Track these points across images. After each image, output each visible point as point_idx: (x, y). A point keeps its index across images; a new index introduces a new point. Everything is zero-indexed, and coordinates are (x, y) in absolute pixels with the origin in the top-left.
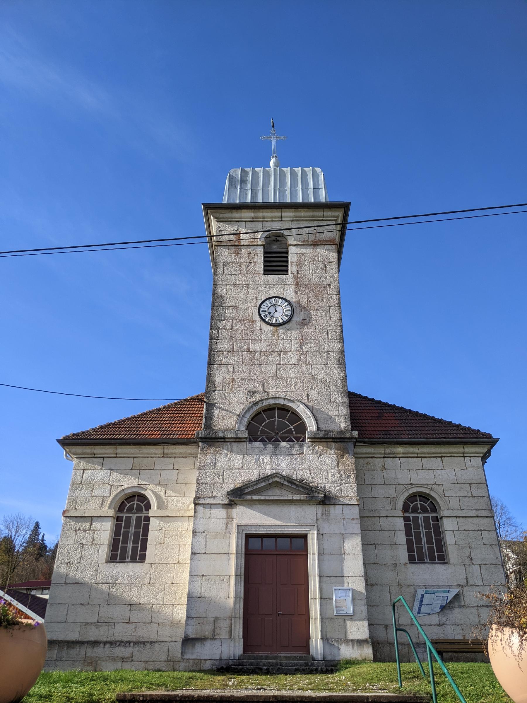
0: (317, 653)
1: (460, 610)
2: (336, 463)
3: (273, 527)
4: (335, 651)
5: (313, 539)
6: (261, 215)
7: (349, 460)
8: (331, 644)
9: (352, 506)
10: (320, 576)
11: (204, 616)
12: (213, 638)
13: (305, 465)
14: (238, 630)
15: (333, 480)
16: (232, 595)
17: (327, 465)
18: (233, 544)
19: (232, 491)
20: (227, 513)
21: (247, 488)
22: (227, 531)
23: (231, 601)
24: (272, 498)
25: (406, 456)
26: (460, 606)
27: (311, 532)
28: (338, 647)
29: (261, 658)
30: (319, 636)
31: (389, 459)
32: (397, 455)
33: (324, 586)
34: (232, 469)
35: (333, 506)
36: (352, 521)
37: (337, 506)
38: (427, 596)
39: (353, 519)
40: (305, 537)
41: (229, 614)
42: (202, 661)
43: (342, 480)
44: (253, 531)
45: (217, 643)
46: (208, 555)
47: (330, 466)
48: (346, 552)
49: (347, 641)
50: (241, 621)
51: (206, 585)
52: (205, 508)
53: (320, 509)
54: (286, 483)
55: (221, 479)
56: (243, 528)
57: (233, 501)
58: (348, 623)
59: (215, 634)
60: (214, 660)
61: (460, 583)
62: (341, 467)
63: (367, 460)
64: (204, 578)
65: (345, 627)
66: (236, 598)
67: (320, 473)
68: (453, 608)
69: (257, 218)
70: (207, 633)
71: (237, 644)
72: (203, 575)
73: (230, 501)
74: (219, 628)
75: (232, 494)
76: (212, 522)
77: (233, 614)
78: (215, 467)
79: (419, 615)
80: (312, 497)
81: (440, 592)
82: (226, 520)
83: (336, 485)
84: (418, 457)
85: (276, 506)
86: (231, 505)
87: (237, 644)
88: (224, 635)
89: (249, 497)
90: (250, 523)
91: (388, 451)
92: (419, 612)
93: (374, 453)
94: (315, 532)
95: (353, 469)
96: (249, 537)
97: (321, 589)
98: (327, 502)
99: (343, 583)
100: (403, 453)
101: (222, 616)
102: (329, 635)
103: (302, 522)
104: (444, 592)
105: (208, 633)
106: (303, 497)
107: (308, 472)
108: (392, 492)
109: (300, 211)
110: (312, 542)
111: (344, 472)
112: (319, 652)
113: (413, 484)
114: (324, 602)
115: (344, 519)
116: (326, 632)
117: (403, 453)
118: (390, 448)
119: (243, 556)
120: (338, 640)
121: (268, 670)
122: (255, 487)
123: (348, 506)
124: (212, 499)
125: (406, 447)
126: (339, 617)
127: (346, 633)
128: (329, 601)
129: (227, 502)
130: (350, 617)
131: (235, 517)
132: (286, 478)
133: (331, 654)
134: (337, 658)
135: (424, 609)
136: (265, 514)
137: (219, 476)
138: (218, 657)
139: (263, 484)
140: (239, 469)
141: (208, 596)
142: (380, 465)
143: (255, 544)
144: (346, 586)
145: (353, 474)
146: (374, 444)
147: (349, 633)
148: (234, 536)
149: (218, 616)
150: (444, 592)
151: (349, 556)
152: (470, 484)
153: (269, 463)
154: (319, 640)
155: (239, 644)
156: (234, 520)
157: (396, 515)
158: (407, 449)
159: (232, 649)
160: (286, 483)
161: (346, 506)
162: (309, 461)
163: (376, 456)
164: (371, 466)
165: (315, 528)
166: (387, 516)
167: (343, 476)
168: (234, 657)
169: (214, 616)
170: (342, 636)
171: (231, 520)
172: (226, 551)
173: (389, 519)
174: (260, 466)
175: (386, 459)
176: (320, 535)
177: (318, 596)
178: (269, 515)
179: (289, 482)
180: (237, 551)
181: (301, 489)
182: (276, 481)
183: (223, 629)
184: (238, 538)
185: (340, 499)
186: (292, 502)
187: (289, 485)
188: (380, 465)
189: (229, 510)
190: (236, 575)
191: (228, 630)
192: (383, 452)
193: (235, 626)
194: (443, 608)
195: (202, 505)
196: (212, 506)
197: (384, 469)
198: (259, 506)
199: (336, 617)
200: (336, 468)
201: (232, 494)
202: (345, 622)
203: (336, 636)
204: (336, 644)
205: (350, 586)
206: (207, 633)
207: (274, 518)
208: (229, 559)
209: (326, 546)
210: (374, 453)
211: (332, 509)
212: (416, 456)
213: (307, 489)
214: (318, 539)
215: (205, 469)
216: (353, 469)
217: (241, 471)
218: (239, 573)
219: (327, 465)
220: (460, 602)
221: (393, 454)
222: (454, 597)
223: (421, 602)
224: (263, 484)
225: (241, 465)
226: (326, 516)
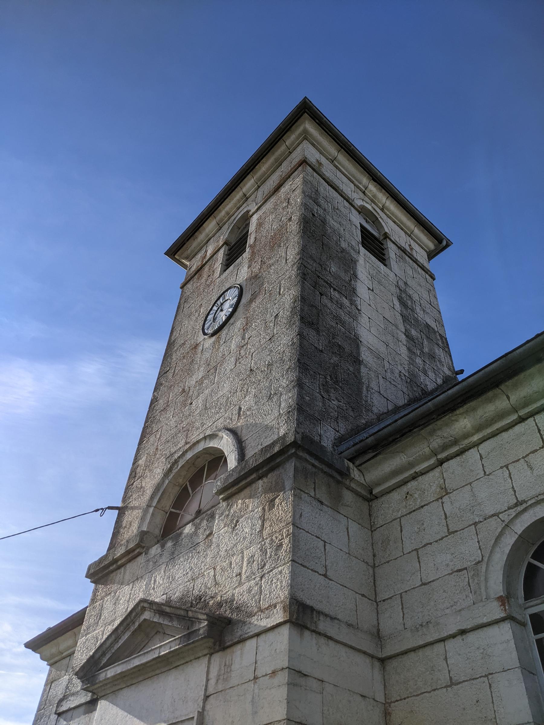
6: (223, 213)
25: (489, 430)
31: (452, 462)
32: (466, 442)
35: (239, 646)
63: (405, 489)
69: (221, 220)
84: (522, 420)
91: (436, 442)
93: (411, 465)
100: (478, 429)
108: (468, 549)
109: (260, 168)
113: (525, 502)
117: (478, 429)
118: (439, 433)
125: (474, 409)
142: (433, 488)
146: (395, 441)
157: (485, 620)
158: (480, 412)
163: (418, 469)
164: (415, 499)
166: (463, 632)
173: (471, 637)
175: (445, 465)
188: (433, 488)
192: (427, 450)
197: (445, 492)
210: (411, 465)
212: (514, 417)
221: (455, 442)
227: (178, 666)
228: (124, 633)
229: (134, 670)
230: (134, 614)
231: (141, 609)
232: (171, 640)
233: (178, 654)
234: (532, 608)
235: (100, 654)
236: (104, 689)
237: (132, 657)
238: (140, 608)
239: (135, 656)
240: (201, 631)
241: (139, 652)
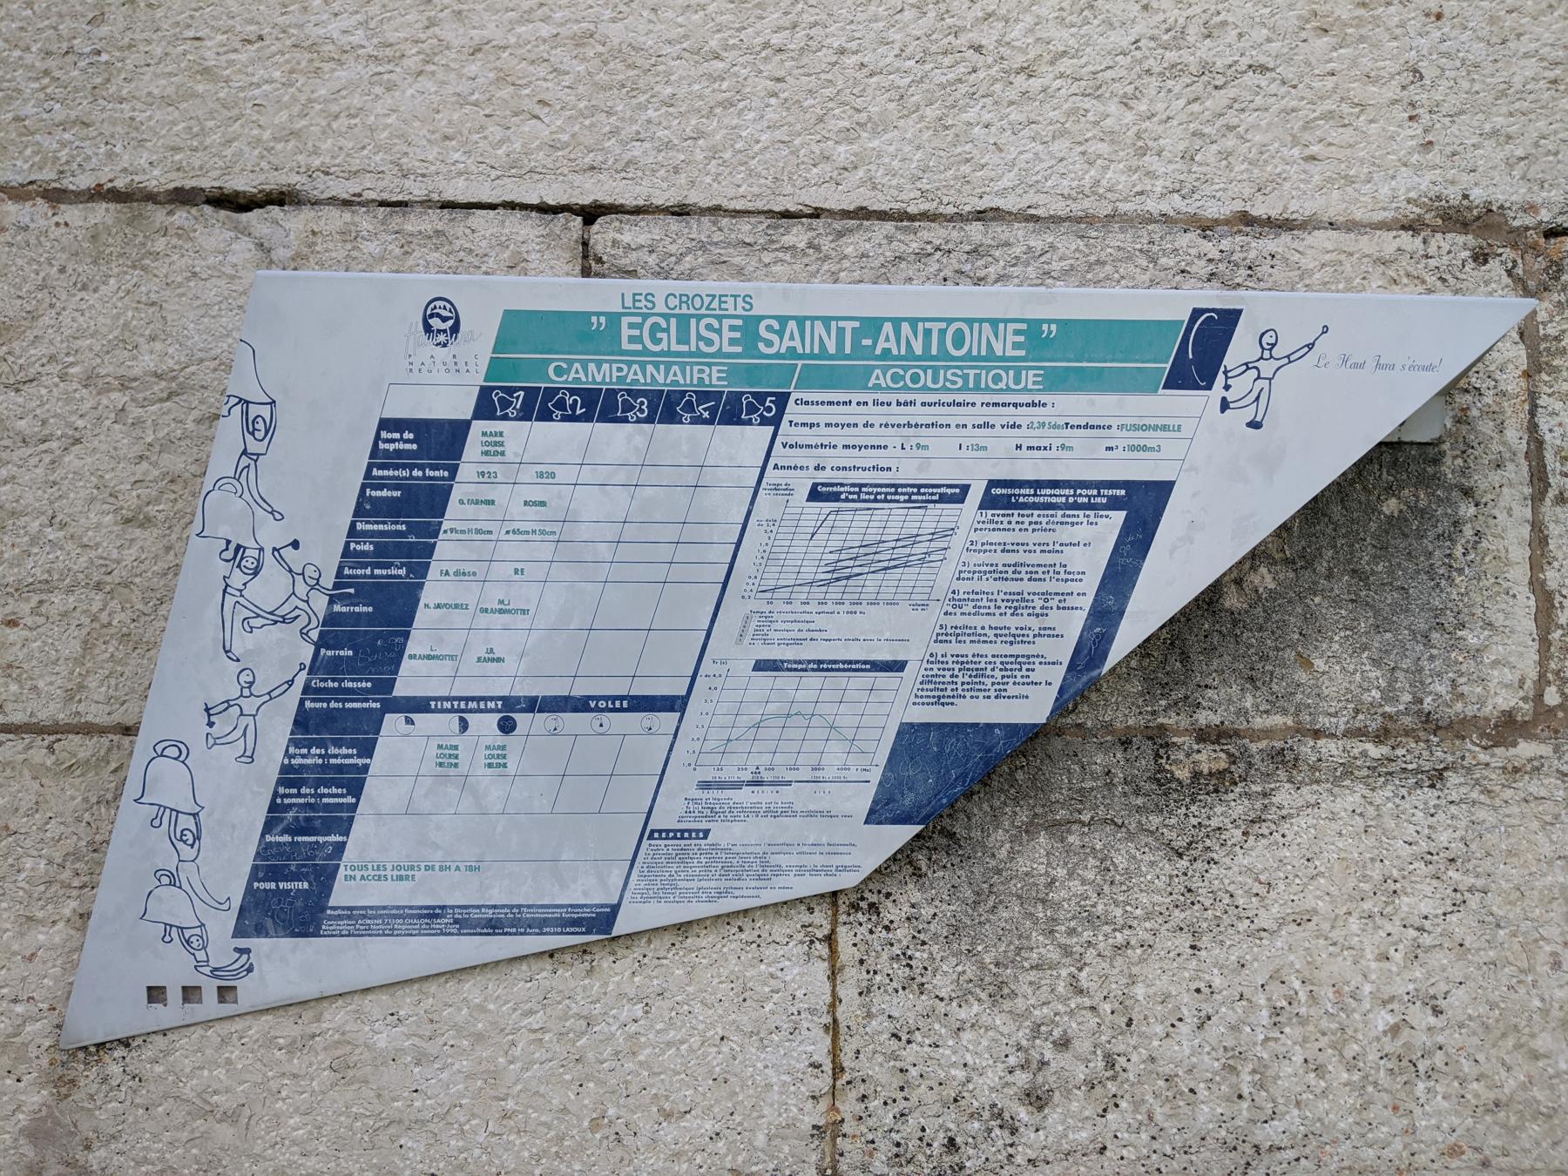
1: (1412, 819)
26: (1425, 739)
38: (520, 478)
61: (1495, 187)
68: (1247, 765)
79: (284, 965)
81: (941, 361)
92: (292, 890)
104: (1072, 355)
106: (1128, 637)
121: (1540, 479)
135: (417, 810)
150: (1072, 355)
194: (955, 788)
220: (1446, 623)
222: (1314, 510)
223: (365, 631)
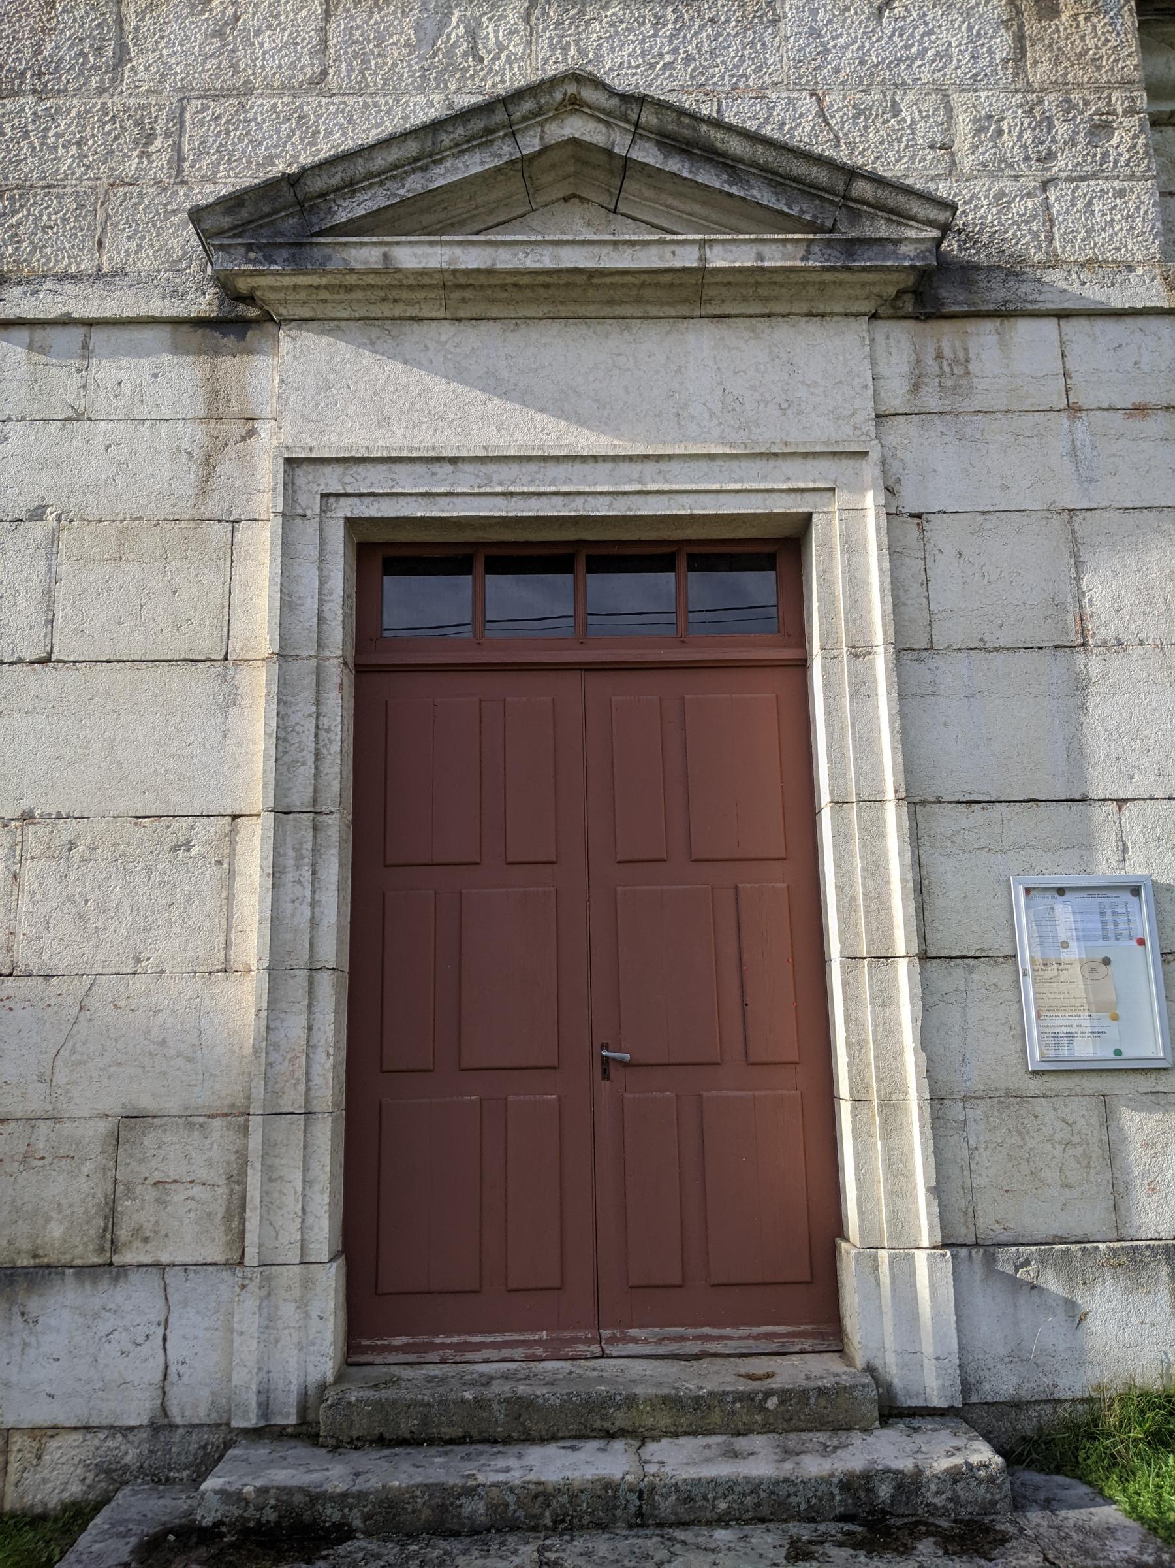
0: (909, 1355)
2: (1002, 44)
3: (552, 470)
4: (1049, 1332)
5: (853, 547)
7: (1100, 22)
8: (1016, 1285)
9: (1129, 322)
10: (915, 803)
11: (35, 1105)
12: (106, 1269)
13: (782, 55)
14: (304, 1205)
15: (986, 153)
16: (252, 946)
17: (944, 55)
18: (261, 591)
19: (234, 202)
20: (213, 391)
21: (350, 187)
22: (214, 505)
23: (245, 996)
24: (548, 264)
27: (840, 499)
28: (1070, 1304)
29: (488, 1380)
30: (925, 1230)
33: (943, 868)
34: (248, 90)
36: (1137, 425)
37: (1024, 328)
39: (1139, 410)
40: (779, 549)
41: (223, 1090)
42: (18, 1442)
43: (1051, 156)
44: (409, 500)
45: (135, 1300)
46: (63, 672)
47: (960, 66)
48: (1100, 632)
49: (1133, 1259)
50: (326, 1138)
51: (51, 880)
52: (44, 350)
53: (899, 344)
54: (648, 154)
55: (161, 161)
56: (331, 479)
57: (248, 299)
58: (1136, 1124)
59: (123, 1234)
60: (113, 1429)
62: (1040, 72)
64: (33, 836)
65: (1112, 1154)
66: (276, 971)
67: (895, 110)
70: (56, 1231)
71: (288, 1311)
72: (27, 817)
73: (224, 284)
74: (150, 1194)
75: (238, 230)
76: (98, 443)
77: (258, 1091)
78: (116, 80)
80: (852, 246)
82: (200, 430)
83: (1009, 186)
85: (576, 330)
86: (237, 321)
87: (288, 1311)
88: (190, 1237)
89: (365, 255)
90: (380, 443)
94: (870, 500)
95: (1126, 83)
96: (388, 554)
97: (921, 891)
98: (952, 297)
99: (1086, 844)
101: (173, 1105)
102: (991, 1218)
103: (767, 436)
105: (63, 1234)
107: (808, 104)
110: (849, 567)
111: (1068, 106)
112: (928, 1348)
114: (951, 978)
115: (1074, 410)
116: (969, 1191)
119: (335, 672)
120: (1058, 1247)
122: (414, 184)
123: (1100, 325)
124: (97, 289)
126: (1061, 1084)
127: (1118, 1195)
128: (983, 974)
129: (204, 304)
130: (1146, 1083)
131: (267, 410)
132: (649, 118)
133: (1016, 1356)
134: (1072, 1383)
136: (494, 385)
137: (151, 137)
138: (136, 1410)
139: (475, 164)
140: (295, 91)
141: (62, 962)
143: (425, 605)
144: (1105, 868)
145: (1131, 111)
147: (1140, 1195)
148: (261, 544)
149: (146, 1103)
151: (1118, 662)
152: (932, 648)
153: (515, 47)
154: (921, 1259)
155: (303, 1305)
156: (264, 429)
159: (247, 1350)
160: (648, 154)
161: (1082, 324)
162: (814, 33)
165: (870, 470)
167: (1062, 130)
168: (265, 1408)
169: (113, 1104)
170: (1089, 1218)
171: (240, 428)
172: (208, 645)
174: (451, 67)
176: (905, 520)
177: (901, 941)
178: (524, 397)
179: (670, 143)
180: (285, 638)
181: (764, 196)
182: (574, 141)
183: (178, 1196)
184: (288, 551)
185: (1049, 276)
186: (691, 296)
187: (675, 165)
189: (226, 364)
190: (281, 812)
191: (217, 1200)
193: (270, 1176)
195: (24, 334)
196: (98, 337)
198: (447, 331)
199: (1036, 1085)
200: (1005, 77)
201: (238, 230)
202: (1108, 1116)
203: (1039, 1217)
204: (1052, 1282)
205: (1136, 868)
206: (56, 1231)
207: (562, 414)
208: (231, 701)
209: (945, 595)
211: (983, 339)
213: (810, 190)
214: (895, 552)
215: (40, 95)
216: (1126, 83)
217: (310, 105)
218: (300, 797)
219: (944, 55)
224: (475, 164)
225: (310, 66)
226: (944, 398)
227: (729, 316)
228: (461, 149)
229: (554, 280)
230: (528, 106)
231: (562, 103)
232: (776, 236)
233: (758, 284)
234: (644, 1353)
235: (336, 180)
236: (325, 301)
237: (445, 238)
238: (558, 96)
239: (457, 238)
240: (904, 249)
241: (477, 233)
